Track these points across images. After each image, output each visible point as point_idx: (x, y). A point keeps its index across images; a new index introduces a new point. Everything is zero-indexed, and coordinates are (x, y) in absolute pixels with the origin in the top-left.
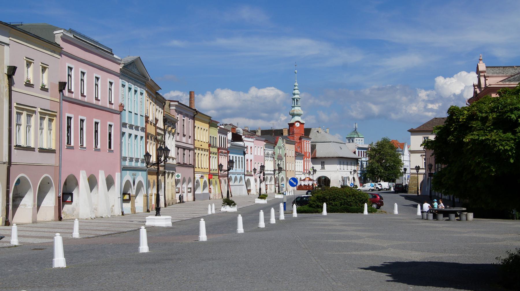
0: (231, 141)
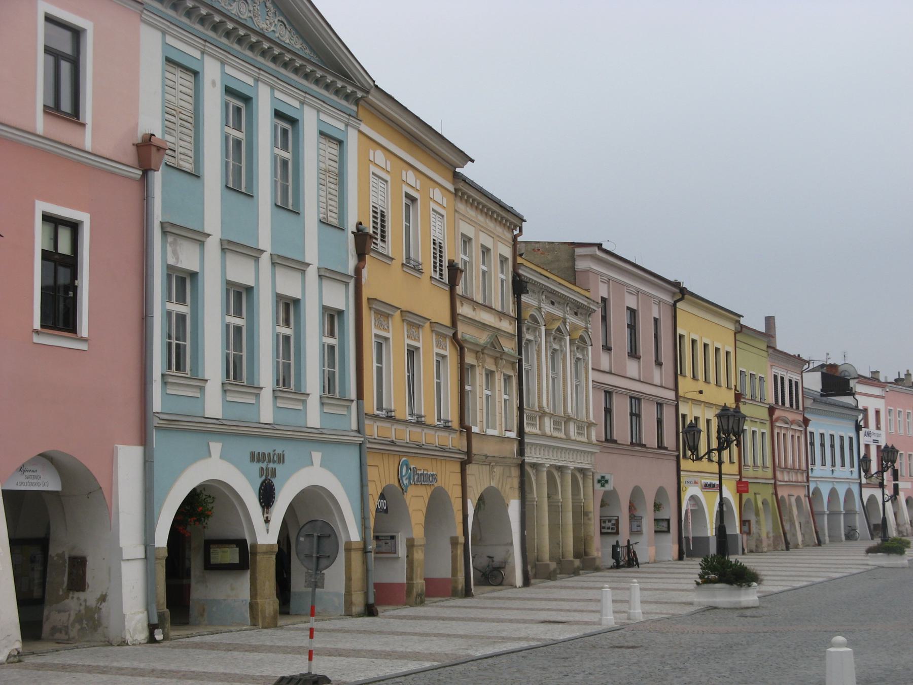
0: (822, 395)
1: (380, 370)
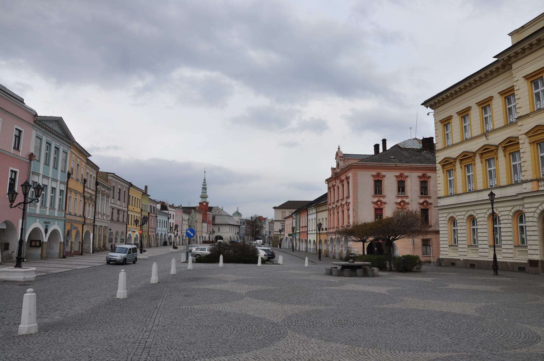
0: (160, 210)
1: (69, 203)
